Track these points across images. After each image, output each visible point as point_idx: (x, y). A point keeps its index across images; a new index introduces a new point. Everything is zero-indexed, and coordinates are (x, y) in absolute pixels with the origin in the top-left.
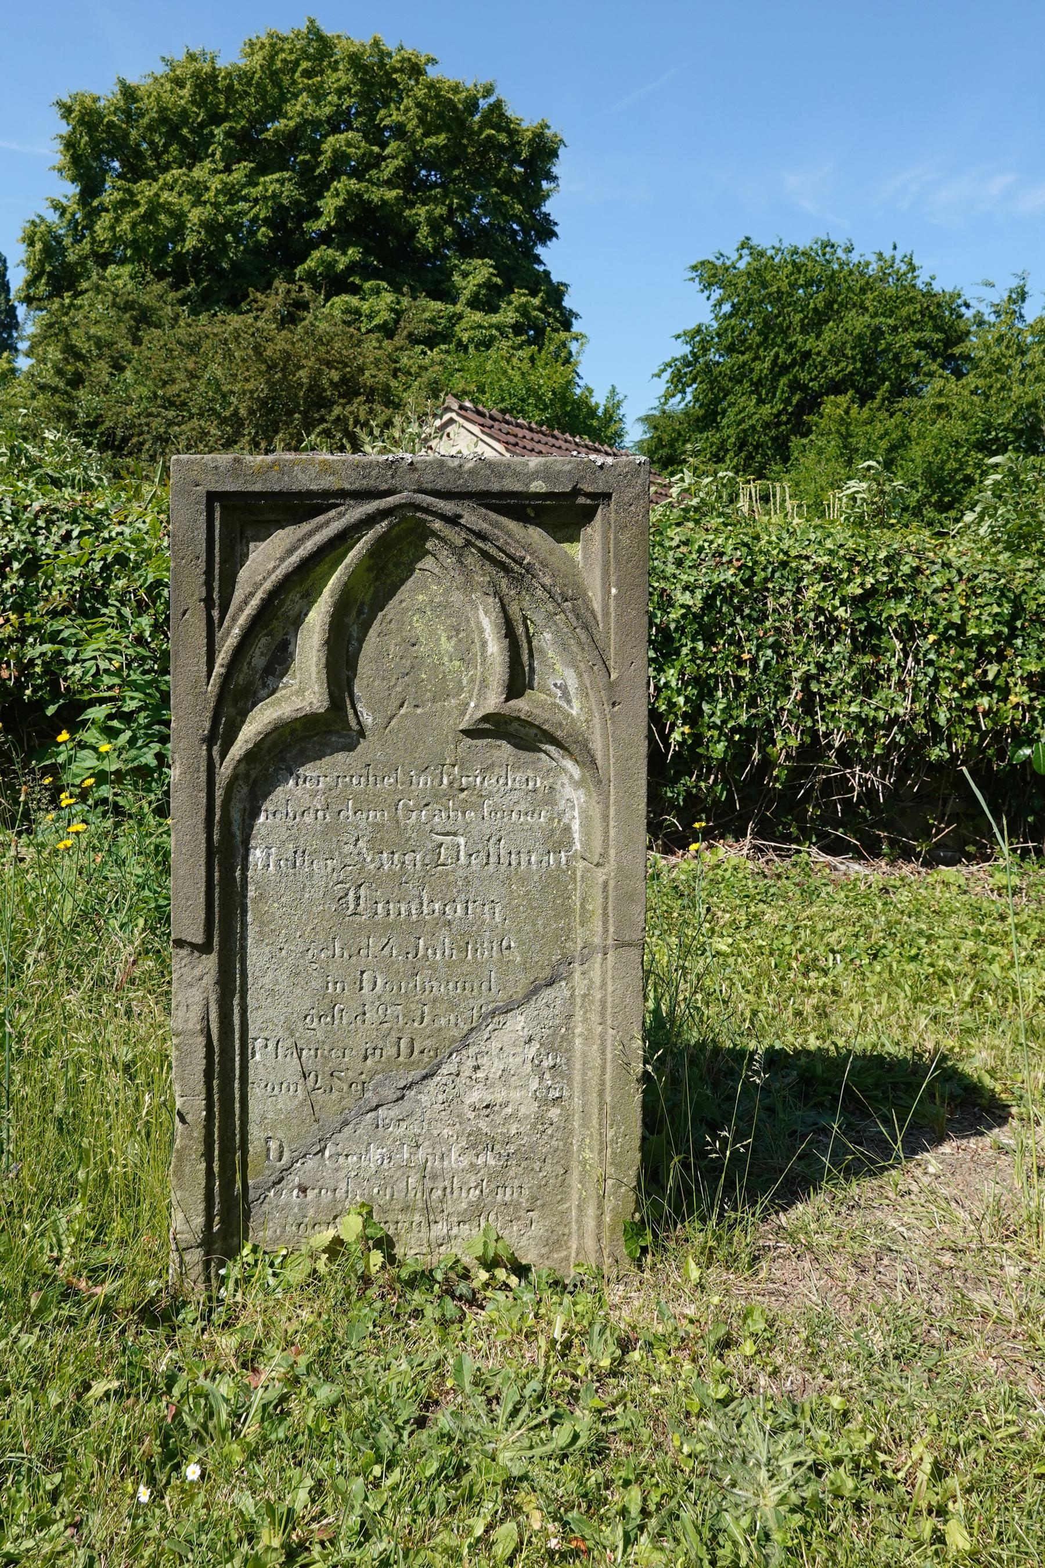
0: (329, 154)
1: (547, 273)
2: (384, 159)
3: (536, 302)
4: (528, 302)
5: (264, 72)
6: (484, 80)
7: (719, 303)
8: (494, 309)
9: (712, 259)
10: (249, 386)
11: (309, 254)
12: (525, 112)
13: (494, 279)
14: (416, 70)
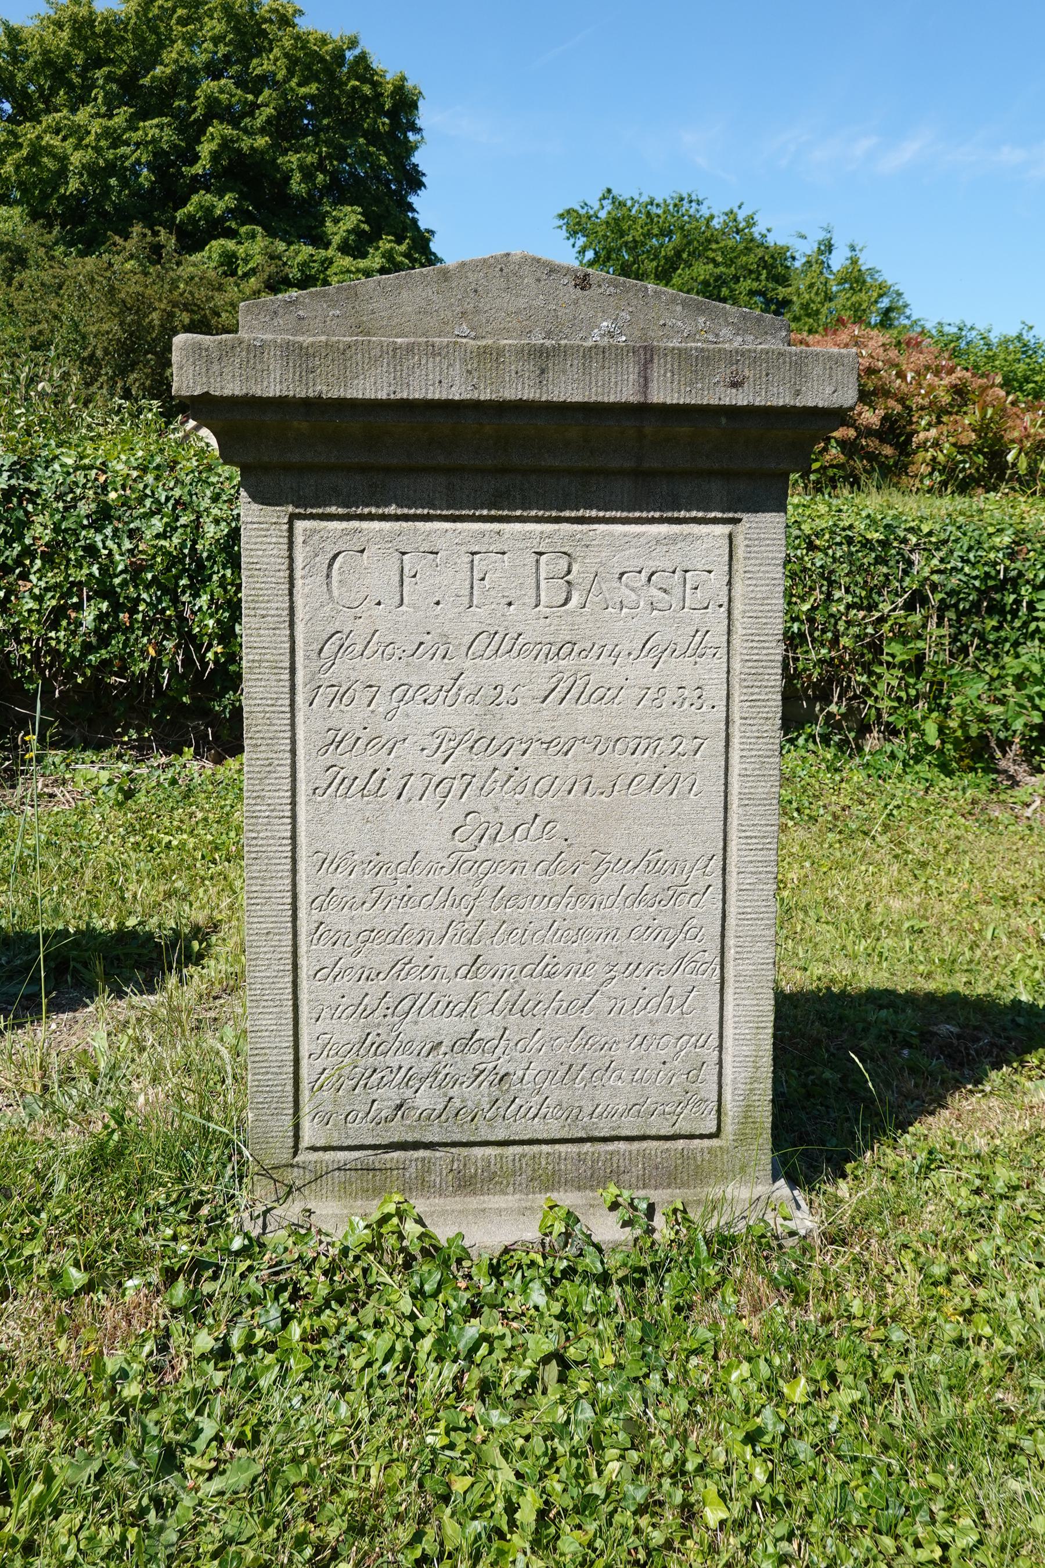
0: (202, 99)
1: (414, 221)
2: (259, 107)
3: (403, 248)
4: (392, 248)
5: (138, 18)
6: (349, 33)
7: (583, 251)
8: (364, 255)
9: (577, 207)
10: (105, 327)
11: (189, 199)
12: (389, 63)
13: (363, 226)
14: (285, 21)
